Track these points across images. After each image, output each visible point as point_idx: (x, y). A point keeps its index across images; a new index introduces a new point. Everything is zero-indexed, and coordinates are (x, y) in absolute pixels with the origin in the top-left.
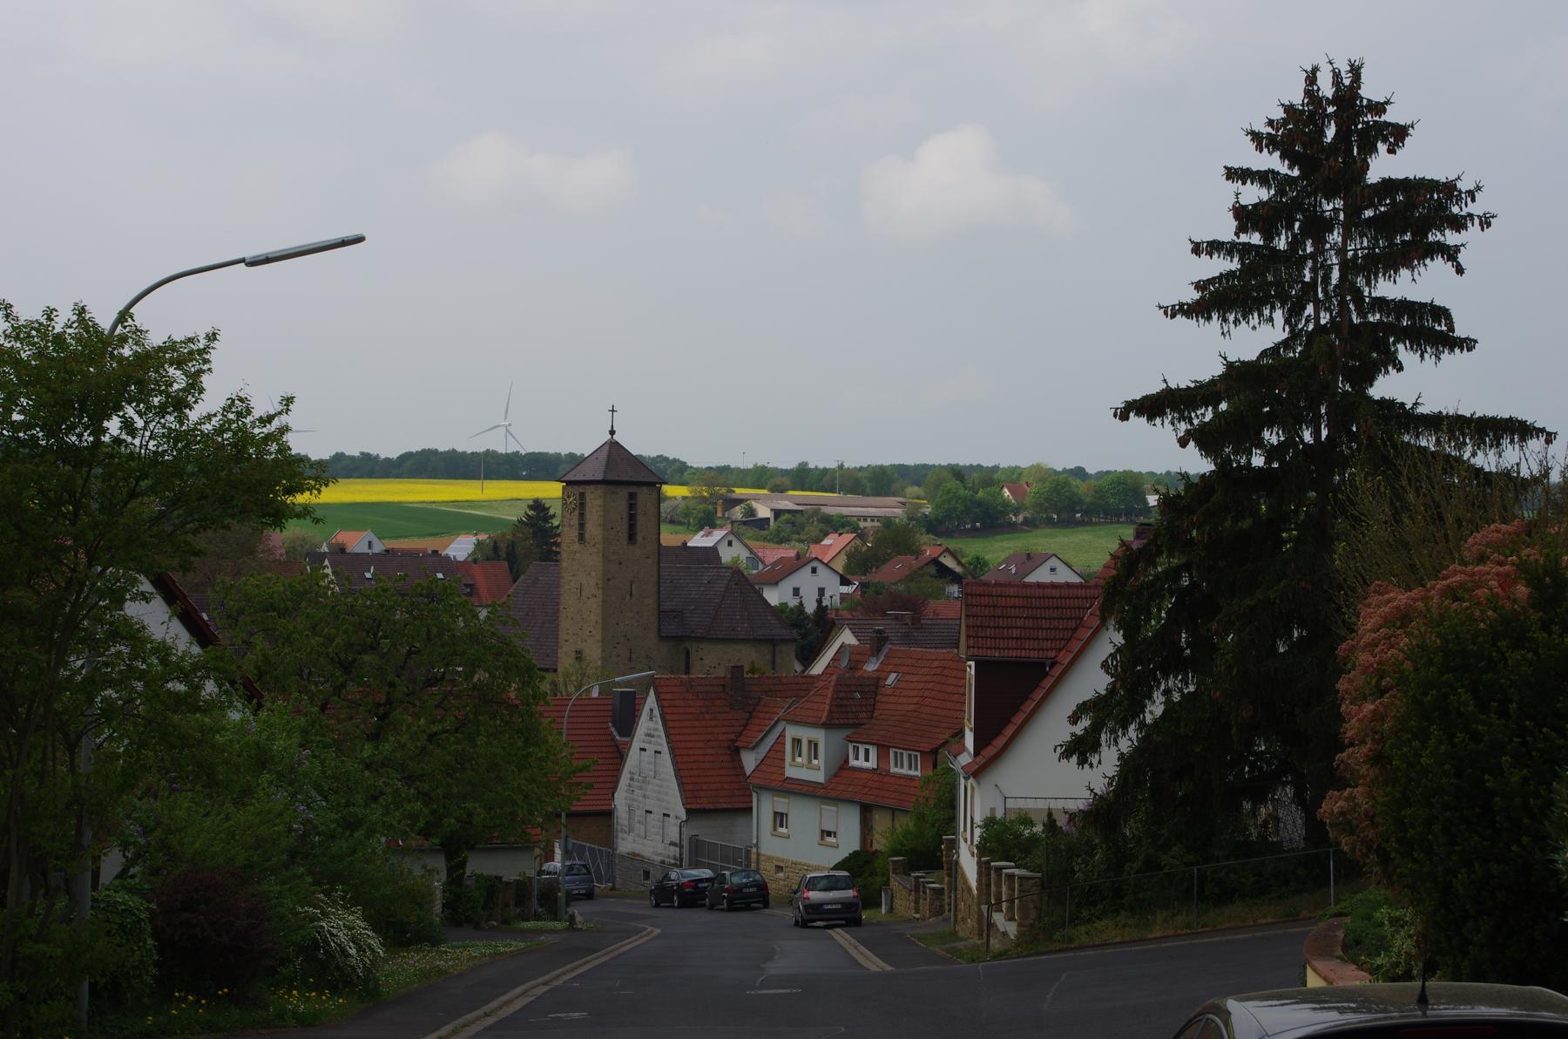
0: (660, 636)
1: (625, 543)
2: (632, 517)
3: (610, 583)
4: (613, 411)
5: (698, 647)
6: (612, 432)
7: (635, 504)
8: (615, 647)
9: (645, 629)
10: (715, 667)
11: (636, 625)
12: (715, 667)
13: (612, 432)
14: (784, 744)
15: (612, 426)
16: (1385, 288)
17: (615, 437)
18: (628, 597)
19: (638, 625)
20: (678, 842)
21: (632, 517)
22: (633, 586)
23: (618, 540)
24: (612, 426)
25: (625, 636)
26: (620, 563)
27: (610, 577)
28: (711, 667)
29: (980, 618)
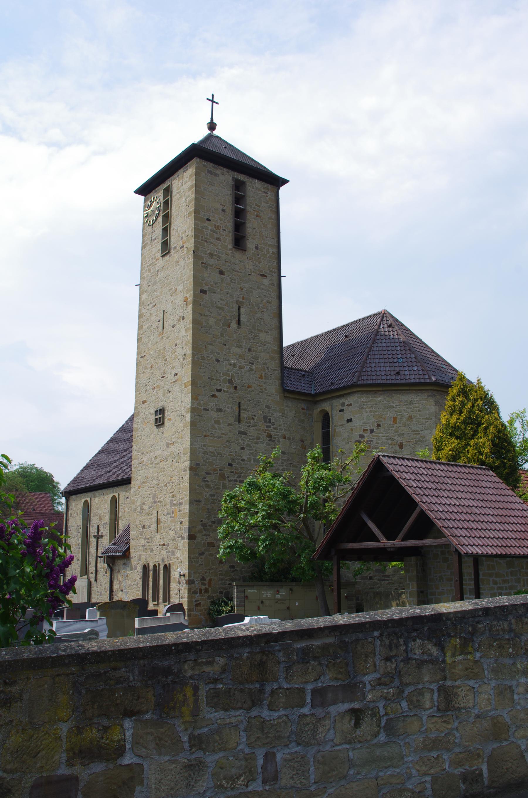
0: (285, 391)
1: (230, 246)
2: (239, 214)
3: (206, 297)
4: (213, 101)
5: (343, 404)
6: (212, 126)
7: (243, 197)
8: (214, 396)
9: (261, 378)
10: (372, 431)
11: (247, 368)
12: (372, 431)
13: (212, 126)
14: (462, 599)
15: (212, 119)
16: (387, 774)
17: (216, 133)
18: (234, 325)
19: (251, 370)
20: (211, 99)
21: (239, 214)
22: (242, 310)
23: (218, 239)
24: (212, 119)
25: (230, 382)
26: (221, 273)
27: (205, 288)
28: (365, 430)
29: (477, 615)
